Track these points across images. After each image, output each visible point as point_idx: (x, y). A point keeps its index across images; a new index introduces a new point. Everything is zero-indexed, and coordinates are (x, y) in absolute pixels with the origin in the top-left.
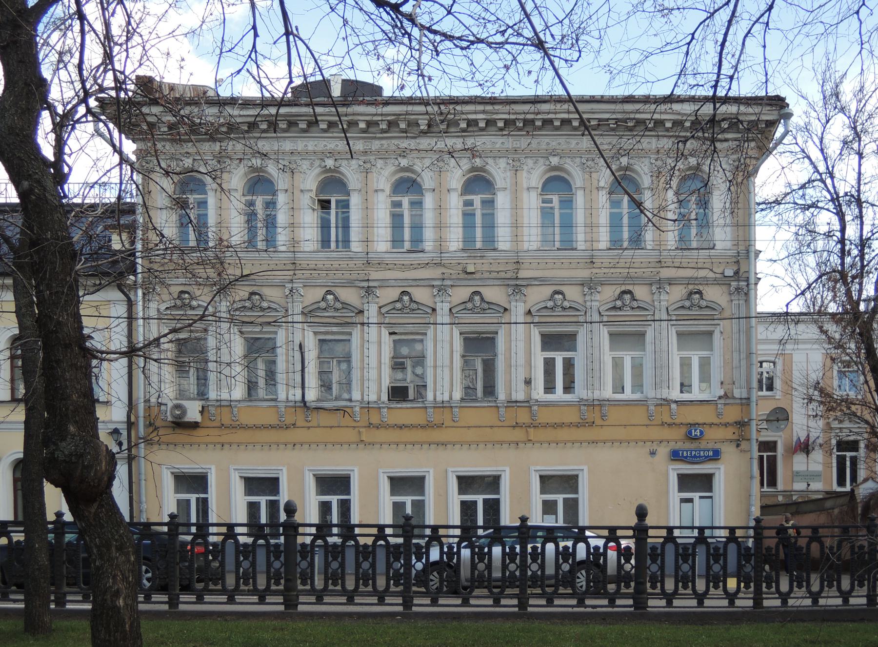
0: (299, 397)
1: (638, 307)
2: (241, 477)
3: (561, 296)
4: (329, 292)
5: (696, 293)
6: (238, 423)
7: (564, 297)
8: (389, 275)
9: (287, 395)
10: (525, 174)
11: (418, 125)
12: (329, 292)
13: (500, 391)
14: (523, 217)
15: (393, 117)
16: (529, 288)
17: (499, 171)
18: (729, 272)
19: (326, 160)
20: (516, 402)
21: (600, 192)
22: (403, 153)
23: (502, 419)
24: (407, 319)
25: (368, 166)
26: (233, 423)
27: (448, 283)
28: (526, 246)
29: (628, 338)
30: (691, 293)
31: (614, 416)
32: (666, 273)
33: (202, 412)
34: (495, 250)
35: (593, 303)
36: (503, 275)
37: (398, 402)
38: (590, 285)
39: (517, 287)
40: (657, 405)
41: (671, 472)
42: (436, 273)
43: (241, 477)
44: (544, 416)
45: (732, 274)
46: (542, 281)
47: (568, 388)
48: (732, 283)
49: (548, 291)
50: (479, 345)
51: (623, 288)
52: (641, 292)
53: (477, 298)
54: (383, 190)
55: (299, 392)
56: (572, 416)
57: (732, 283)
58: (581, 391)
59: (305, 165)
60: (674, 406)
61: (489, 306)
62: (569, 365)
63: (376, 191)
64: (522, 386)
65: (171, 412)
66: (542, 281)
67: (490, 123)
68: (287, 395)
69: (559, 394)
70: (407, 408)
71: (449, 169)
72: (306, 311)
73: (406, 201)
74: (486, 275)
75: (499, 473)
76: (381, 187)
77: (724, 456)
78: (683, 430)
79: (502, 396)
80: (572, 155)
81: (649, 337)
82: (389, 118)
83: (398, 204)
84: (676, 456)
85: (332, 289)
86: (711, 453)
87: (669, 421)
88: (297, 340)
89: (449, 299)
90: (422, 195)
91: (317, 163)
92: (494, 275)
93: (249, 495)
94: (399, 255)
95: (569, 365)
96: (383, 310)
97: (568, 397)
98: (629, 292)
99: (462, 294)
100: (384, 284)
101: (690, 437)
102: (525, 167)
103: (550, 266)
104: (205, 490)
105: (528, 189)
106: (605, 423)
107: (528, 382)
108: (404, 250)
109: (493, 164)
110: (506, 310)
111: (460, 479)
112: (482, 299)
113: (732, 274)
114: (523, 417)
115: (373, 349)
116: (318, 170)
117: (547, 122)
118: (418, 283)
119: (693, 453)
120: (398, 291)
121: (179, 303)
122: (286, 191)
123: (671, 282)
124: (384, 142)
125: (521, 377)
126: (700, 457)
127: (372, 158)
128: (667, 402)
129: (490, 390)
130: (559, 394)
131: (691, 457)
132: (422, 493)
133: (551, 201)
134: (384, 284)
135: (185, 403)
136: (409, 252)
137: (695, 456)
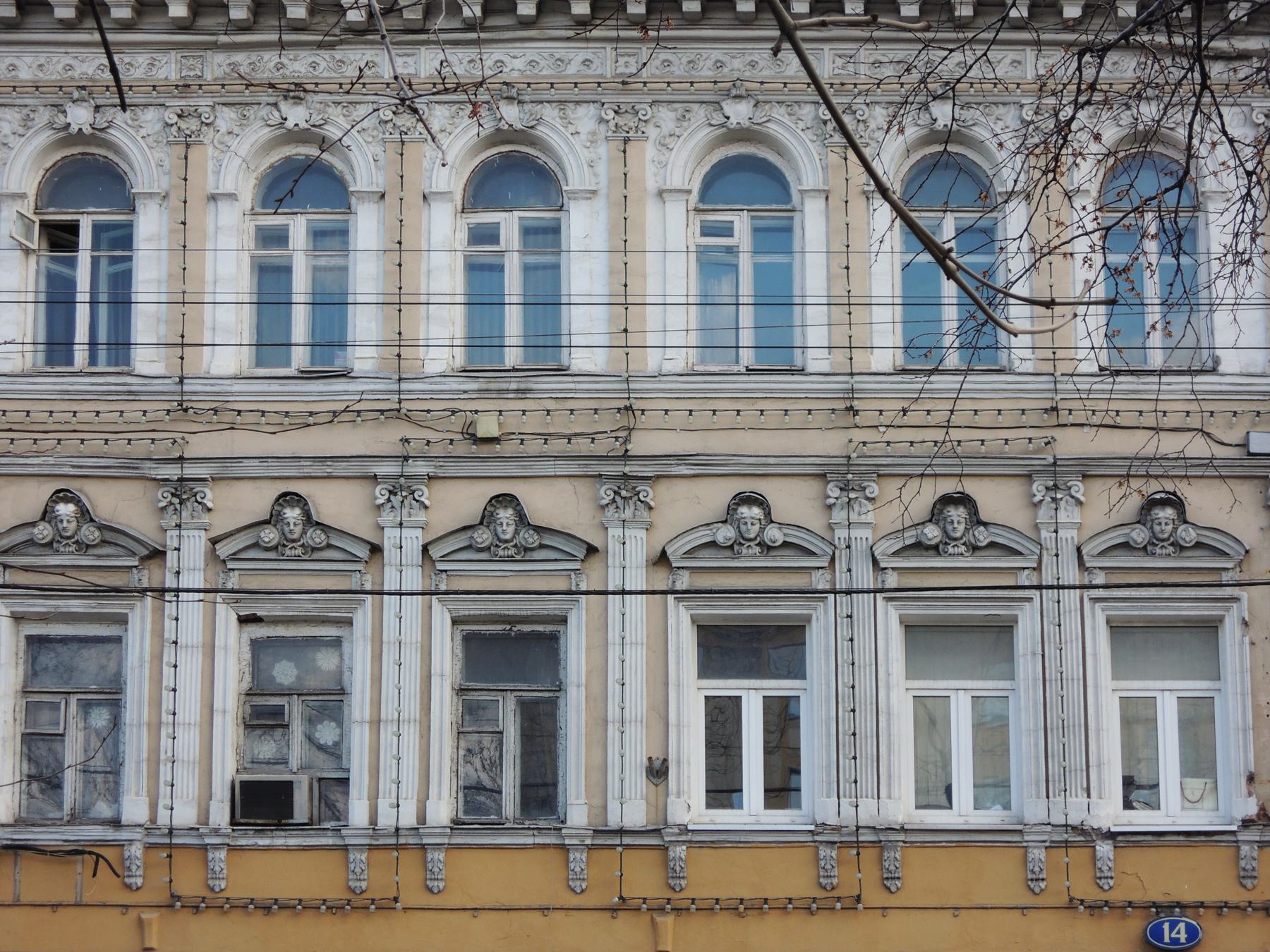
1: (992, 545)
5: (1163, 503)
10: (650, 151)
14: (644, 276)
16: (663, 487)
17: (141, 147)
20: (621, 832)
22: (296, 91)
25: (193, 124)
27: (421, 468)
28: (653, 360)
29: (961, 638)
30: (1151, 504)
32: (1072, 444)
34: (561, 371)
36: (583, 446)
38: (844, 478)
39: (627, 483)
40: (1052, 846)
42: (386, 438)
44: (708, 877)
46: (702, 466)
47: (781, 791)
50: (512, 657)
51: (948, 487)
52: (999, 500)
54: (232, 196)
56: (793, 879)
58: (818, 801)
60: (1104, 849)
61: (540, 540)
62: (782, 719)
63: (213, 198)
64: (638, 781)
66: (702, 466)
73: (742, 224)
74: (534, 447)
76: (227, 186)
79: (577, 814)
80: (567, 95)
83: (276, 238)
85: (72, 485)
87: (1092, 895)
89: (421, 516)
90: (349, 210)
91: (43, 116)
92: (558, 446)
94: (275, 386)
96: (224, 550)
97: (781, 818)
99: (457, 502)
100: (228, 470)
102: (652, 132)
103: (724, 420)
107: (658, 772)
114: (643, 879)
115: (191, 665)
116: (46, 137)
118: (328, 467)
120: (50, 487)
123: (1088, 469)
124: (239, 57)
127: (204, 103)
128: (1084, 836)
129: (541, 794)
133: (727, 230)
134: (228, 470)
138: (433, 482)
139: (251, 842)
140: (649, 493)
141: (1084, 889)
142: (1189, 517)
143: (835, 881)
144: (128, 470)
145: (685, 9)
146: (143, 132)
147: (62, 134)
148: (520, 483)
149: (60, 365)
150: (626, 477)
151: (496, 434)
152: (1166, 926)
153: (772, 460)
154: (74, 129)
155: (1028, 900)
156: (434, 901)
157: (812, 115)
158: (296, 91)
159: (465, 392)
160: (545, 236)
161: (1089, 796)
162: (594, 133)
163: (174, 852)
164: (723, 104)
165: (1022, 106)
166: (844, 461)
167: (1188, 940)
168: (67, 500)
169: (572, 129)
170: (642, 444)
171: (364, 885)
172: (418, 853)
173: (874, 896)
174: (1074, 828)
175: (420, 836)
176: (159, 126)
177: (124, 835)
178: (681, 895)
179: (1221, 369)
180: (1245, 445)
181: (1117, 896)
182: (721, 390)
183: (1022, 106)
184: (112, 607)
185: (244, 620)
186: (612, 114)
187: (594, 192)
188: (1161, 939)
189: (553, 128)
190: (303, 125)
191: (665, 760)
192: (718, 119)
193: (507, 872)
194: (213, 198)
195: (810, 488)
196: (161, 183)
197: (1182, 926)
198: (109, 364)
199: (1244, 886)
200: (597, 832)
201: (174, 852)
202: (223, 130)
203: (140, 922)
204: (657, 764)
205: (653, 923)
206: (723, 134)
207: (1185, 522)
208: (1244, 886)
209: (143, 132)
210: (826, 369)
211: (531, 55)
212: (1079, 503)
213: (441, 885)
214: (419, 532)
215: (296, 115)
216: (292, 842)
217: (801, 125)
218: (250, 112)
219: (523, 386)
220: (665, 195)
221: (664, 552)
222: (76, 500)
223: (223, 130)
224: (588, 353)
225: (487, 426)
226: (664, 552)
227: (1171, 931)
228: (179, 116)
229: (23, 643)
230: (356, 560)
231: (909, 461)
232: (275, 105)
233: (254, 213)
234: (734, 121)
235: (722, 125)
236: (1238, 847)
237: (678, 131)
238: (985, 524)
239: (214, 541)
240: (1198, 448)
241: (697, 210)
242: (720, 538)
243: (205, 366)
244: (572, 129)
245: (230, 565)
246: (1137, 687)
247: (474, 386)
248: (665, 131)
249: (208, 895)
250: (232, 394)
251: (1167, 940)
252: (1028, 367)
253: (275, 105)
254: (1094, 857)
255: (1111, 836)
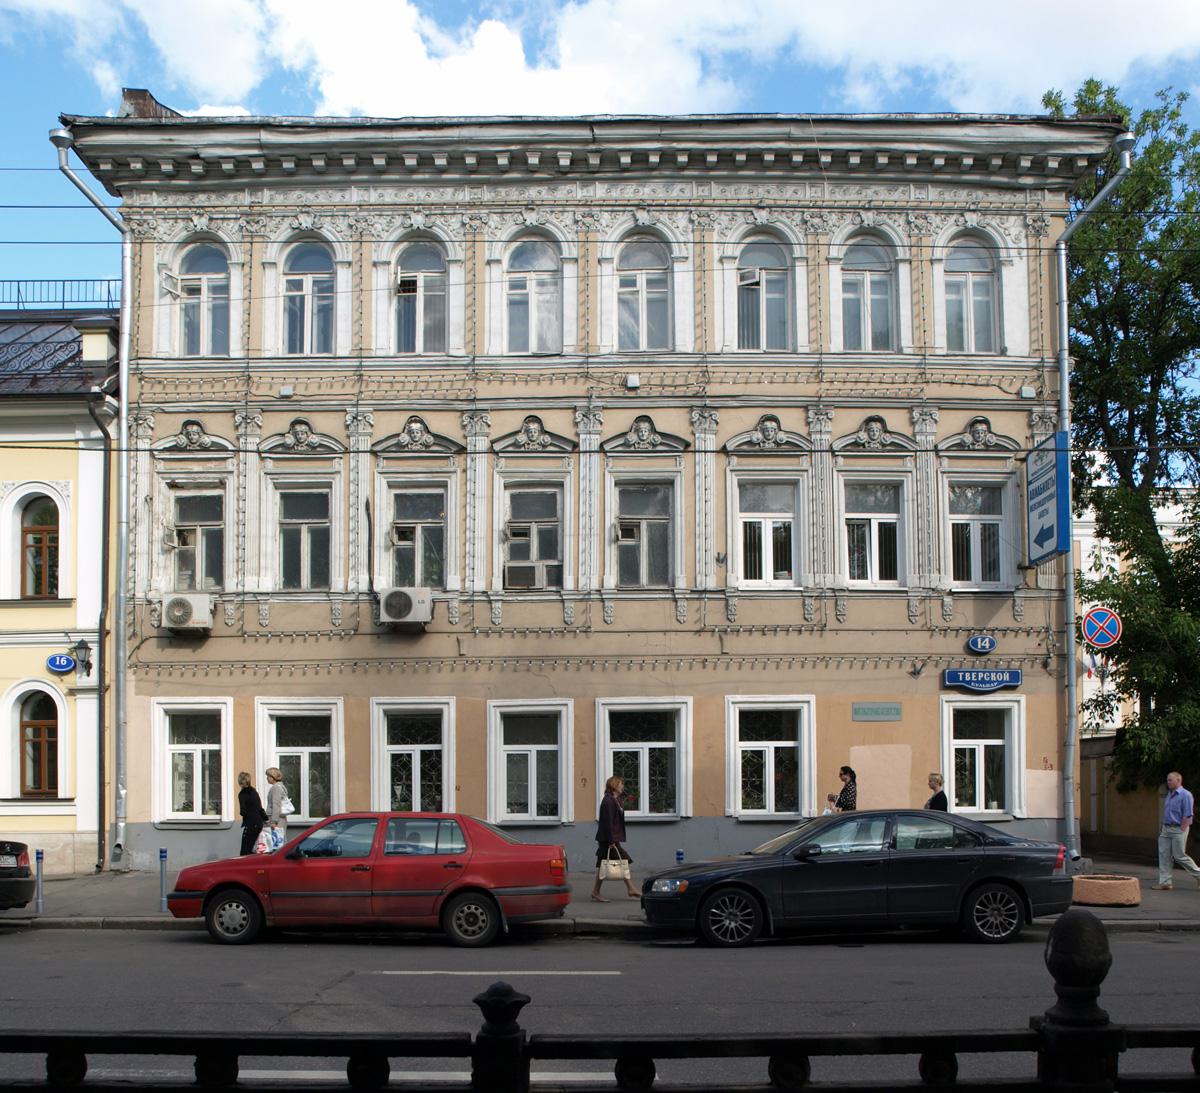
0: (364, 587)
1: (892, 444)
2: (271, 716)
3: (774, 424)
4: (413, 420)
5: (981, 422)
6: (269, 629)
7: (779, 426)
8: (507, 390)
9: (346, 583)
11: (556, 160)
12: (413, 420)
13: (678, 573)
14: (713, 302)
15: (518, 147)
17: (676, 227)
18: (1029, 391)
19: (413, 215)
20: (705, 591)
21: (726, 266)
22: (530, 206)
23: (681, 619)
24: (767, 459)
25: (477, 223)
26: (260, 629)
30: (974, 423)
31: (856, 612)
33: (214, 612)
34: (673, 353)
35: (824, 437)
37: (519, 592)
38: (816, 407)
39: (703, 407)
40: (924, 599)
41: (946, 705)
42: (581, 388)
43: (271, 716)
44: (746, 614)
45: (1033, 395)
46: (743, 402)
48: (1035, 409)
49: (752, 417)
50: (645, 497)
52: (896, 420)
53: (645, 426)
54: (498, 261)
55: (364, 577)
56: (791, 613)
57: (1035, 409)
58: (806, 574)
59: (379, 224)
60: (948, 600)
62: (888, 533)
63: (375, 264)
64: (713, 566)
65: (168, 612)
66: (743, 402)
67: (668, 158)
68: (346, 583)
69: (874, 580)
70: (532, 601)
71: (599, 227)
72: (497, 447)
73: (308, 281)
75: (677, 706)
76: (496, 256)
77: (1025, 682)
78: (962, 639)
79: (682, 583)
80: (673, 207)
81: (805, 483)
82: (513, 148)
83: (298, 285)
84: (952, 682)
85: (420, 414)
86: (1007, 677)
87: (942, 624)
88: (364, 492)
89: (599, 428)
90: (446, 272)
91: (398, 221)
93: (287, 744)
94: (523, 361)
95: (888, 533)
96: (497, 447)
98: (880, 420)
99: (618, 421)
100: (500, 404)
101: (971, 650)
102: (716, 227)
104: (216, 738)
105: (721, 260)
106: (840, 626)
107: (722, 560)
108: (530, 353)
109: (668, 222)
110: (688, 445)
111: (615, 717)
112: (653, 430)
113: (1033, 395)
114: (714, 615)
115: (481, 509)
117: (755, 158)
118: (553, 402)
119: (981, 675)
120: (407, 416)
121: (968, 438)
122: (243, 265)
125: (714, 550)
126: (990, 682)
127: (484, 211)
128: (935, 593)
129: (662, 571)
130: (768, 580)
131: (977, 682)
132: (554, 740)
133: (633, 283)
134: (500, 404)
135: (190, 598)
136: (765, 353)
137: (983, 681)
138: (265, 414)
139: (514, 598)
140: (719, 415)
141: (937, 620)
142: (993, 430)
143: (572, 619)
144: (445, 407)
145: (530, 162)
146: (451, 228)
147: (409, 230)
148: (421, 413)
149: (430, 351)
150: (705, 406)
151: (638, 384)
152: (979, 640)
153: (780, 399)
154: (415, 226)
155: (911, 626)
156: (608, 628)
157: (800, 218)
158: (306, 209)
159: (621, 363)
160: (326, 289)
161: (259, 576)
162: (687, 227)
163: (475, 605)
164: (754, 212)
165: (691, 212)
166: (816, 399)
167: (990, 647)
168: (416, 421)
169: (675, 225)
170: (713, 389)
171: (267, 622)
172: (487, 605)
173: (832, 623)
174: (933, 590)
175: (601, 595)
176: (458, 225)
177: (449, 596)
178: (734, 624)
179: (1008, 353)
180: (1019, 393)
181: (954, 625)
182: (775, 362)
183: (691, 212)
184: (332, 476)
185: (391, 486)
186: (696, 217)
187: (687, 258)
188: (977, 647)
189: (665, 225)
190: (535, 223)
191: (726, 554)
192: (751, 219)
193: (644, 611)
194: (489, 263)
195: (799, 414)
196: (242, 258)
197: (987, 640)
198: (319, 352)
199: (1016, 620)
200: (693, 592)
201: (475, 605)
202: (493, 227)
203: (458, 640)
204: (722, 557)
205: (721, 639)
206: (523, 229)
207: (990, 432)
208: (1016, 620)
209: (451, 228)
210: (808, 351)
211: (653, 186)
212: (936, 421)
213: (267, 622)
214: (597, 436)
215: (531, 218)
216: (535, 598)
217: (794, 223)
218: (507, 217)
219: (651, 360)
220: (724, 260)
221: (725, 447)
222: (421, 422)
223: (493, 227)
224: (685, 339)
225: (634, 380)
226: (725, 447)
227: (982, 641)
228: (470, 219)
229: (393, 498)
230: (566, 452)
231: (850, 399)
232: (521, 213)
233: (285, 274)
234: (304, 225)
235: (754, 223)
236: (727, 600)
237: (837, 224)
238: (890, 432)
239: (493, 442)
240: (993, 393)
241: (618, 270)
242: (755, 439)
243: (486, 352)
244: (675, 225)
245: (500, 455)
246: (752, 517)
247: (627, 360)
248: (723, 226)
249: (492, 626)
250: (500, 365)
251: (979, 646)
252: (910, 351)
253: (521, 213)
254: (943, 605)
255: (951, 593)
